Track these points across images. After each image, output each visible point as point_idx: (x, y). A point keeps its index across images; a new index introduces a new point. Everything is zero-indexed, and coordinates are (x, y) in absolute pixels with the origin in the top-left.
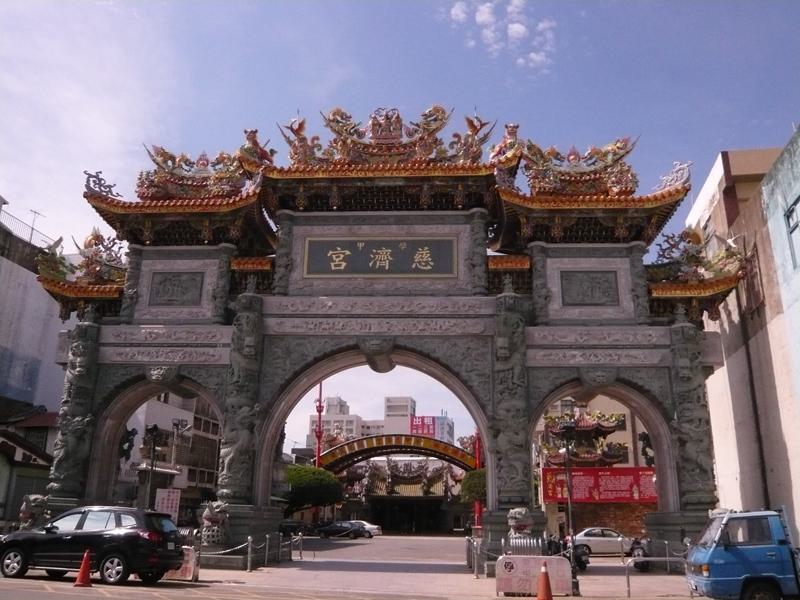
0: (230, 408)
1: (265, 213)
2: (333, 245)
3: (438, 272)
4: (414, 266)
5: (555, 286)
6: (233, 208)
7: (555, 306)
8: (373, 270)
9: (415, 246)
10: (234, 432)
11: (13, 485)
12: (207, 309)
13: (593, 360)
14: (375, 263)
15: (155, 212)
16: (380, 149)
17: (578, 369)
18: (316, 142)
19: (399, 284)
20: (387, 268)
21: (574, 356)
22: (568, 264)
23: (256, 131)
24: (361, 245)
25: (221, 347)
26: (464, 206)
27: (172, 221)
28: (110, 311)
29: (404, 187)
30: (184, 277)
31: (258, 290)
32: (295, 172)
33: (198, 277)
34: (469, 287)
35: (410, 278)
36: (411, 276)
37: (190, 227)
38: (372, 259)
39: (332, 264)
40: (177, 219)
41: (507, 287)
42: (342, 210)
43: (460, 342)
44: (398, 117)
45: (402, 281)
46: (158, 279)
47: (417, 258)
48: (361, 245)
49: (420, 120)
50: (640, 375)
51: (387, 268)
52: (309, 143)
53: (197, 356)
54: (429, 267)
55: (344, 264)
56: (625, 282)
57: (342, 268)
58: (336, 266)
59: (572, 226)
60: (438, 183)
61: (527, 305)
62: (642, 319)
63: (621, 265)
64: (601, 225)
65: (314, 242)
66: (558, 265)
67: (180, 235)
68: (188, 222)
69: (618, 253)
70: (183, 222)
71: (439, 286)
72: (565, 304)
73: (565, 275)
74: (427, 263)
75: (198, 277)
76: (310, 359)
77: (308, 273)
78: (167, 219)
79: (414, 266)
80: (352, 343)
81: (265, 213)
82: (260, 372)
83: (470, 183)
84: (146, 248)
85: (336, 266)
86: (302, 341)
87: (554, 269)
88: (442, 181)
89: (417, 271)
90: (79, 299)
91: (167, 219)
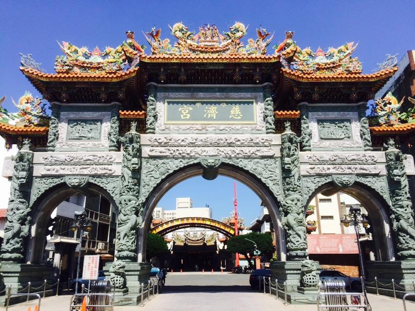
14: (207, 115)
34: (264, 129)
35: (229, 124)
36: (227, 122)
39: (182, 116)
43: (262, 161)
50: (368, 180)
54: (240, 118)
57: (188, 118)
85: (184, 116)
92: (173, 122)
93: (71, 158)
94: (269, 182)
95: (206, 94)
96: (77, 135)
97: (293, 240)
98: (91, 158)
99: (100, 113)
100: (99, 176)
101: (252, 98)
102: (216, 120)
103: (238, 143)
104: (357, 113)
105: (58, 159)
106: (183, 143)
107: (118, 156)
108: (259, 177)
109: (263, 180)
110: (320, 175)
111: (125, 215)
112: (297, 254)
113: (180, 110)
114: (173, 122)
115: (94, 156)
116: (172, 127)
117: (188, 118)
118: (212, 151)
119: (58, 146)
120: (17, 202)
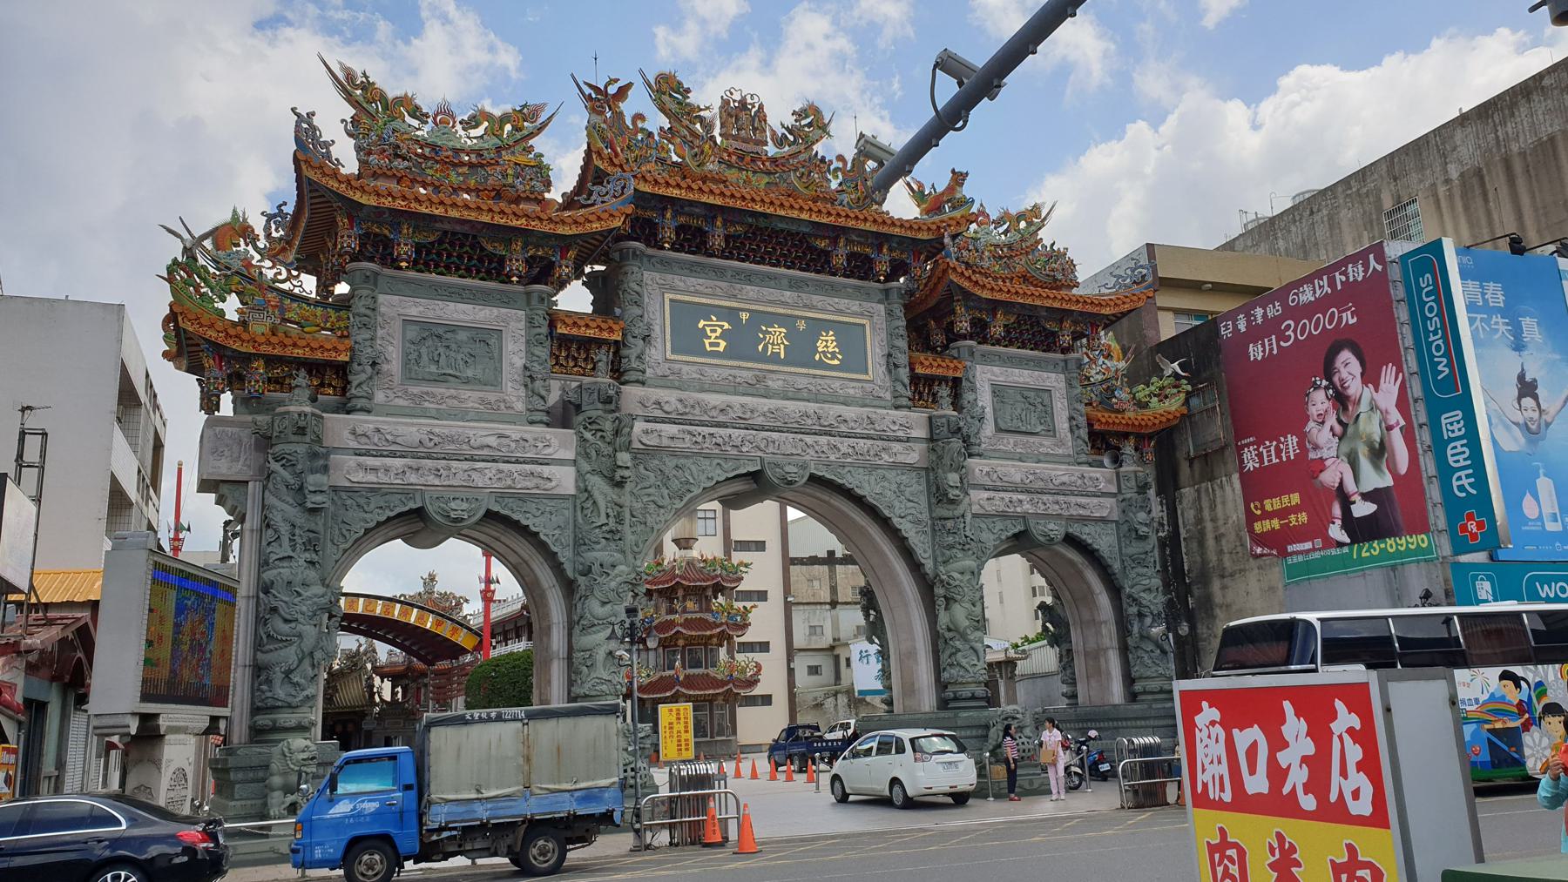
0: (596, 568)
2: (706, 311)
3: (731, 358)
5: (985, 399)
8: (763, 358)
9: (818, 327)
10: (609, 607)
11: (1299, 667)
13: (1041, 509)
14: (766, 347)
15: (437, 212)
16: (741, 158)
17: (1024, 517)
18: (640, 125)
19: (802, 383)
23: (953, 171)
24: (744, 316)
25: (557, 467)
29: (810, 235)
30: (462, 336)
33: (486, 339)
34: (888, 396)
35: (815, 376)
36: (812, 371)
39: (707, 342)
40: (458, 228)
42: (677, 250)
43: (891, 475)
44: (761, 107)
45: (801, 377)
46: (413, 333)
47: (820, 346)
48: (744, 316)
49: (790, 121)
50: (1086, 530)
52: (629, 122)
53: (518, 477)
54: (836, 362)
55: (723, 344)
56: (514, 354)
57: (721, 349)
59: (432, 244)
62: (1083, 458)
68: (475, 237)
71: (852, 392)
72: (999, 430)
73: (998, 391)
75: (486, 339)
77: (673, 352)
85: (711, 344)
86: (682, 461)
89: (821, 365)
90: (257, 356)
92: (685, 358)
93: (436, 440)
94: (909, 525)
95: (765, 291)
96: (433, 368)
97: (964, 662)
98: (493, 441)
99: (495, 310)
100: (522, 498)
101: (862, 315)
102: (785, 362)
103: (843, 428)
104: (354, 111)
105: (399, 440)
106: (721, 418)
107: (561, 443)
108: (887, 513)
109: (895, 520)
110: (1003, 516)
111: (604, 603)
112: (274, 722)
113: (700, 325)
114: (685, 358)
115: (501, 436)
116: (686, 368)
117: (721, 349)
118: (787, 442)
119: (380, 397)
120: (301, 562)
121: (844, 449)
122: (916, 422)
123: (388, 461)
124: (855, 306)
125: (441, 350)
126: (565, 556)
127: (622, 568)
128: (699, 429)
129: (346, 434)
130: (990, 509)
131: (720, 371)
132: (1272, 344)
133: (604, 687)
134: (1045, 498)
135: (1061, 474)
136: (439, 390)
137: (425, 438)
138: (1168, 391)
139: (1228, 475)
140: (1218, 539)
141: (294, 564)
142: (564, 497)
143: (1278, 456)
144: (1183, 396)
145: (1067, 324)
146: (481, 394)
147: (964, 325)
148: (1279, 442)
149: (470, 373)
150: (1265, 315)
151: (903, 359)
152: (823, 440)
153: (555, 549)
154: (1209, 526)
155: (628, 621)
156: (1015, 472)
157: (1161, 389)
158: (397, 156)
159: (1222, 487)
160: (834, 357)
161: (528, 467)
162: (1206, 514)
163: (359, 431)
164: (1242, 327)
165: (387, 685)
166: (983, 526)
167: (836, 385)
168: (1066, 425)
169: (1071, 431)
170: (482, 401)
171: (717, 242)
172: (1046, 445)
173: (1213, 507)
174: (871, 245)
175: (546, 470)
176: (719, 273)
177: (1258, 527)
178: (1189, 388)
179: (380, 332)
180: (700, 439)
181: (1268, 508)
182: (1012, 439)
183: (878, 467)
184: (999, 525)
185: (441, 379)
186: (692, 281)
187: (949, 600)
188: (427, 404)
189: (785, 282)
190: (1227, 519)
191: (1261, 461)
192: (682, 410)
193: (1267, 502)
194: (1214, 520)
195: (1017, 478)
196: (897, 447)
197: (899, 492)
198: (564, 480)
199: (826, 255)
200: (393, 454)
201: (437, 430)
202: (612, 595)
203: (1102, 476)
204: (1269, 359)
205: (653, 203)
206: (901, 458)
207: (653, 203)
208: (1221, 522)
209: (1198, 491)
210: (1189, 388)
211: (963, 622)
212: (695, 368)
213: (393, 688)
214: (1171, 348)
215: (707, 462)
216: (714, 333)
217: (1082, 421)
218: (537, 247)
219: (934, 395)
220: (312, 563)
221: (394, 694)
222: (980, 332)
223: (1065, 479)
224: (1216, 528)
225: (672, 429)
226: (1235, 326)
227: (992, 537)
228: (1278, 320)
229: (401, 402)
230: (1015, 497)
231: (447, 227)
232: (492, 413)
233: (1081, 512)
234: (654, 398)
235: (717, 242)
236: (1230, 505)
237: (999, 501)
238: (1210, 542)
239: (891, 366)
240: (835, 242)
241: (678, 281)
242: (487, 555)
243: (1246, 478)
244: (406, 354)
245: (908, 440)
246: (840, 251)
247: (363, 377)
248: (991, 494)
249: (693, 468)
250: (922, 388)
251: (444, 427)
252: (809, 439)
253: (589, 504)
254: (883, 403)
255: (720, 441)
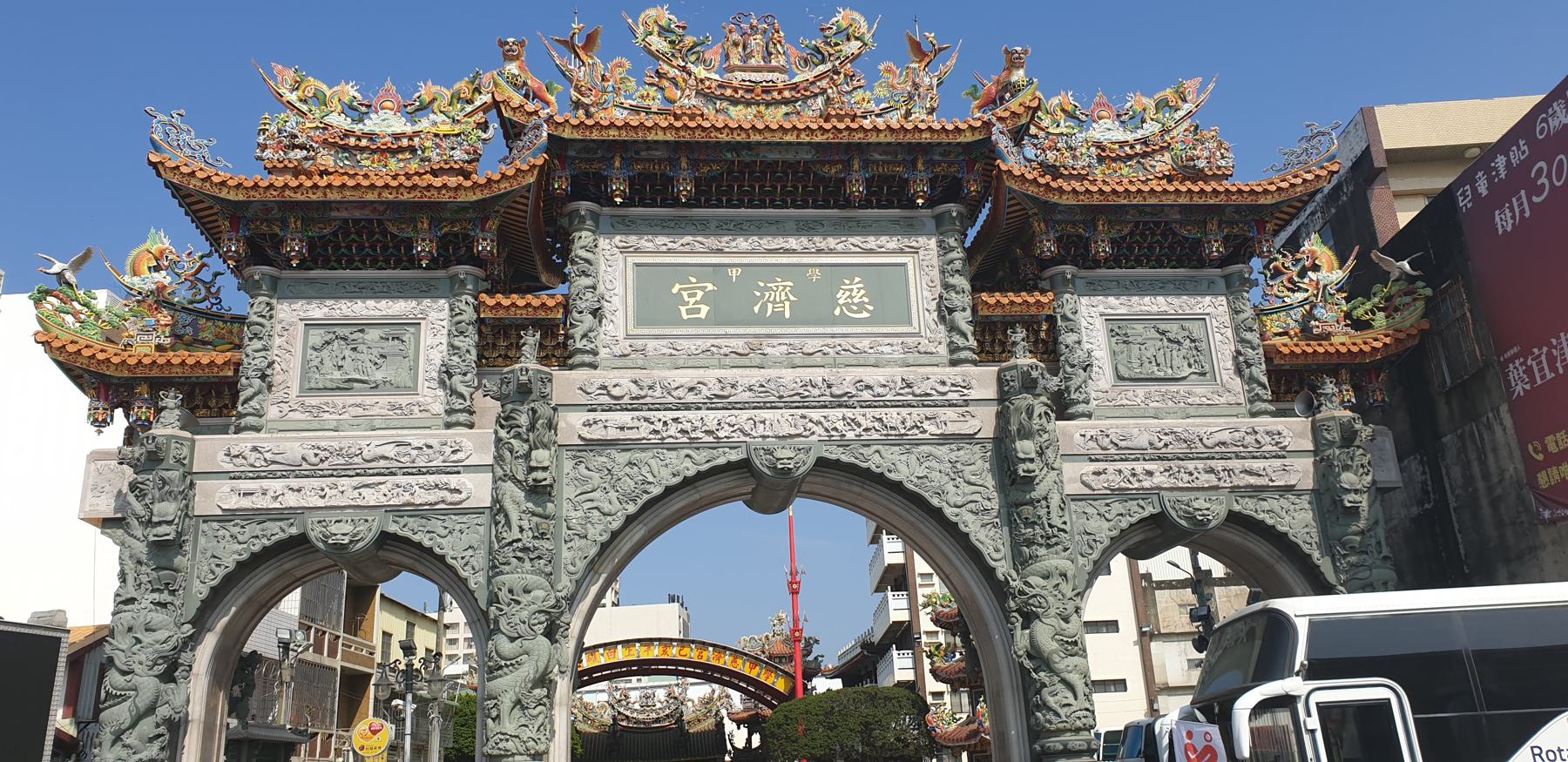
1: (988, 205)
4: (837, 312)
6: (486, 194)
7: (1102, 380)
8: (761, 320)
12: (435, 400)
14: (764, 308)
15: (314, 198)
20: (787, 315)
21: (1150, 473)
22: (1117, 305)
26: (926, 200)
27: (346, 221)
28: (206, 406)
29: (814, 162)
31: (544, 360)
32: (607, 128)
34: (943, 350)
35: (833, 336)
36: (829, 330)
37: (384, 232)
38: (758, 299)
39: (683, 309)
40: (357, 214)
41: (1019, 349)
43: (942, 451)
46: (317, 337)
51: (787, 315)
54: (865, 315)
57: (703, 315)
58: (689, 312)
60: (877, 157)
61: (1054, 383)
63: (1214, 307)
64: (1174, 234)
65: (906, 272)
66: (1101, 309)
67: (361, 248)
68: (380, 222)
69: (1209, 289)
70: (370, 221)
74: (861, 307)
76: (656, 491)
78: (334, 214)
79: (837, 312)
80: (734, 456)
81: (988, 205)
82: (1011, 524)
83: (937, 157)
84: (286, 274)
86: (639, 455)
87: (1091, 318)
88: (884, 153)
91: (334, 214)
93: (323, 454)
94: (969, 518)
96: (337, 375)
97: (1051, 701)
98: (390, 451)
101: (901, 251)
103: (866, 395)
106: (691, 398)
108: (935, 501)
110: (1121, 494)
111: (512, 640)
113: (675, 290)
115: (400, 444)
116: (652, 344)
118: (781, 421)
119: (273, 412)
120: (145, 603)
121: (865, 423)
122: (982, 380)
123: (265, 483)
124: (893, 243)
125: (347, 353)
126: (476, 581)
127: (540, 593)
128: (659, 414)
129: (221, 456)
130: (1099, 484)
131: (699, 342)
132: (1522, 203)
133: (510, 745)
134: (1190, 465)
135: (1214, 429)
136: (340, 400)
137: (310, 454)
138: (1397, 301)
139: (1496, 410)
140: (1495, 503)
141: (135, 606)
142: (478, 511)
143: (1553, 369)
144: (1420, 305)
145: (1213, 226)
146: (392, 399)
147: (1049, 247)
148: (1551, 346)
149: (378, 376)
150: (1508, 164)
151: (962, 300)
152: (839, 412)
153: (464, 574)
154: (1480, 484)
155: (404, 662)
156: (1141, 433)
157: (1388, 299)
158: (295, 147)
159: (1489, 427)
160: (861, 307)
161: (432, 479)
162: (1476, 469)
163: (234, 452)
164: (1483, 189)
165: (744, 731)
166: (1090, 510)
167: (865, 343)
168: (1229, 364)
169: (1239, 372)
170: (393, 407)
171: (685, 188)
172: (1200, 392)
173: (1483, 462)
174: (903, 163)
175: (453, 480)
176: (702, 227)
177: (1543, 479)
178: (1429, 292)
179: (278, 341)
180: (659, 426)
181: (1552, 448)
182: (1141, 391)
183: (918, 443)
184: (1117, 507)
185: (346, 386)
186: (661, 240)
187: (1029, 618)
188: (326, 416)
189: (792, 225)
190: (1502, 472)
191: (1533, 380)
192: (635, 391)
193: (1549, 439)
194: (1486, 476)
195: (1143, 441)
196: (950, 413)
197: (956, 472)
198: (477, 489)
199: (1197, 244)
200: (273, 475)
201: (323, 444)
202: (523, 628)
203: (1295, 430)
204: (1522, 225)
205: (600, 154)
206: (951, 429)
207: (600, 154)
208: (1495, 479)
209: (1461, 438)
210: (1429, 292)
211: (1048, 644)
212: (664, 342)
213: (750, 735)
214: (1402, 243)
215: (674, 454)
216: (693, 299)
217: (1256, 355)
218: (453, 222)
219: (1002, 344)
220: (163, 605)
221: (749, 741)
222: (1077, 252)
223: (1225, 436)
224: (1490, 489)
225: (625, 418)
226: (1474, 190)
227: (1107, 525)
228: (1527, 165)
229: (297, 416)
230: (1139, 467)
231: (345, 214)
232: (401, 419)
233: (1253, 480)
234: (600, 382)
235: (685, 188)
236: (1503, 452)
237: (1114, 475)
238: (1486, 510)
239: (945, 313)
240: (847, 166)
241: (645, 243)
242: (442, 591)
243: (1517, 406)
244: (306, 362)
245: (966, 403)
246: (855, 176)
247: (250, 392)
248: (1100, 466)
249: (652, 462)
250: (991, 339)
251: (329, 441)
252: (816, 414)
253: (500, 518)
254: (934, 360)
255: (688, 426)
